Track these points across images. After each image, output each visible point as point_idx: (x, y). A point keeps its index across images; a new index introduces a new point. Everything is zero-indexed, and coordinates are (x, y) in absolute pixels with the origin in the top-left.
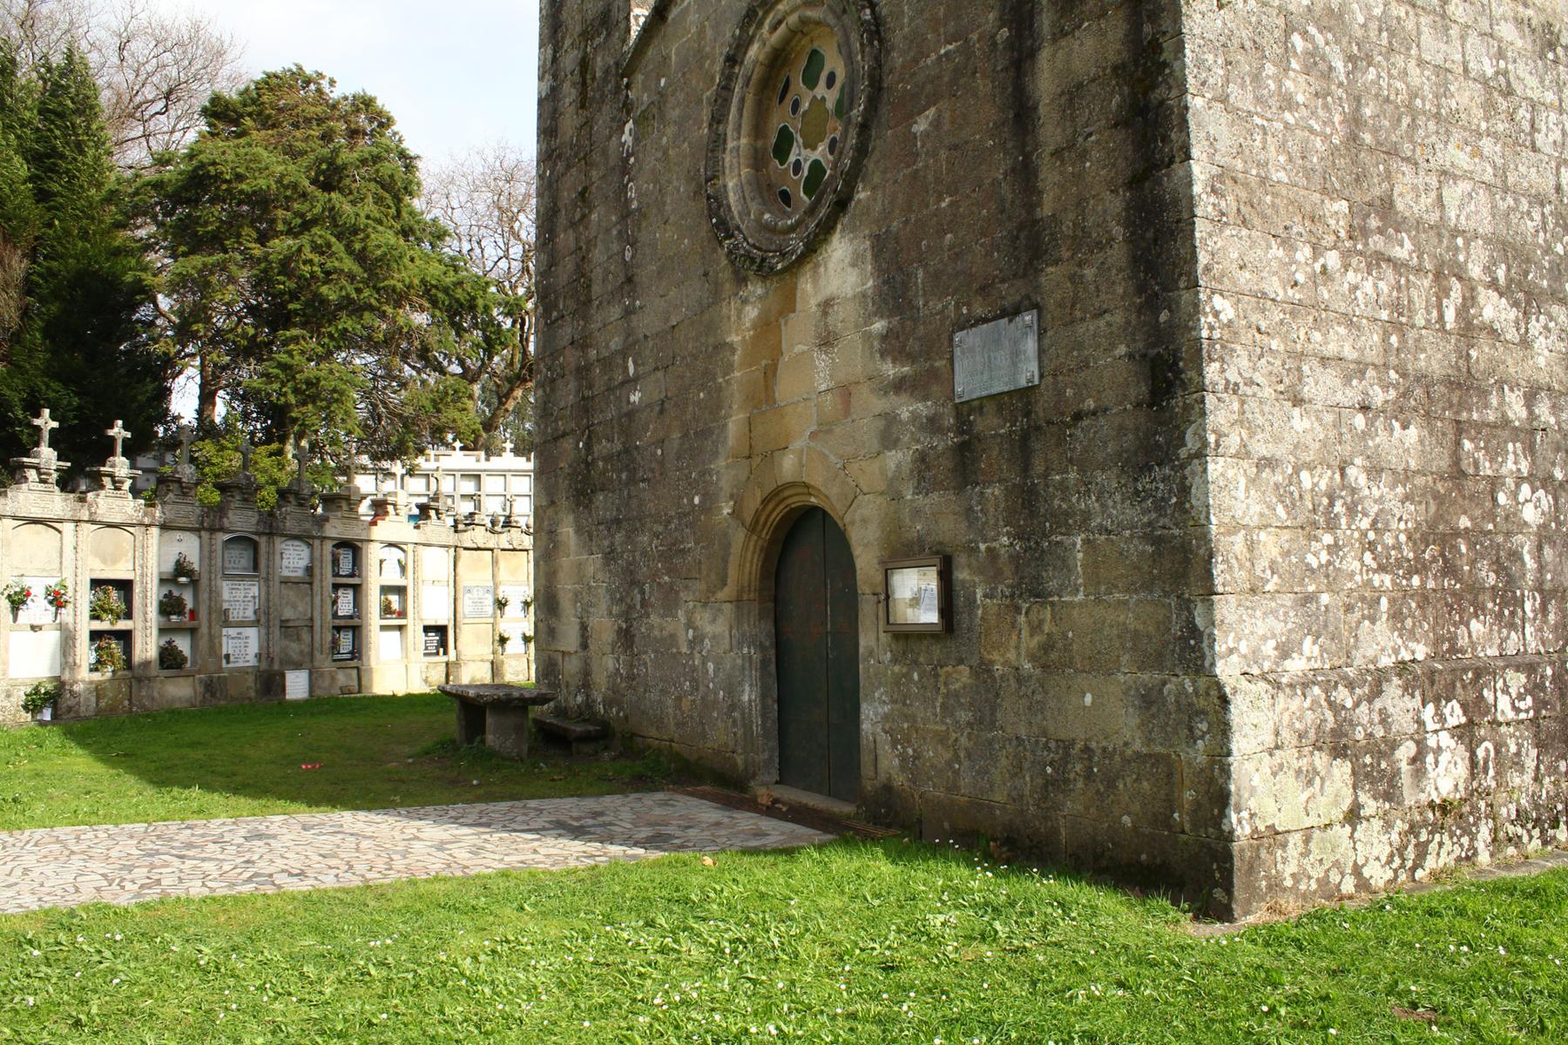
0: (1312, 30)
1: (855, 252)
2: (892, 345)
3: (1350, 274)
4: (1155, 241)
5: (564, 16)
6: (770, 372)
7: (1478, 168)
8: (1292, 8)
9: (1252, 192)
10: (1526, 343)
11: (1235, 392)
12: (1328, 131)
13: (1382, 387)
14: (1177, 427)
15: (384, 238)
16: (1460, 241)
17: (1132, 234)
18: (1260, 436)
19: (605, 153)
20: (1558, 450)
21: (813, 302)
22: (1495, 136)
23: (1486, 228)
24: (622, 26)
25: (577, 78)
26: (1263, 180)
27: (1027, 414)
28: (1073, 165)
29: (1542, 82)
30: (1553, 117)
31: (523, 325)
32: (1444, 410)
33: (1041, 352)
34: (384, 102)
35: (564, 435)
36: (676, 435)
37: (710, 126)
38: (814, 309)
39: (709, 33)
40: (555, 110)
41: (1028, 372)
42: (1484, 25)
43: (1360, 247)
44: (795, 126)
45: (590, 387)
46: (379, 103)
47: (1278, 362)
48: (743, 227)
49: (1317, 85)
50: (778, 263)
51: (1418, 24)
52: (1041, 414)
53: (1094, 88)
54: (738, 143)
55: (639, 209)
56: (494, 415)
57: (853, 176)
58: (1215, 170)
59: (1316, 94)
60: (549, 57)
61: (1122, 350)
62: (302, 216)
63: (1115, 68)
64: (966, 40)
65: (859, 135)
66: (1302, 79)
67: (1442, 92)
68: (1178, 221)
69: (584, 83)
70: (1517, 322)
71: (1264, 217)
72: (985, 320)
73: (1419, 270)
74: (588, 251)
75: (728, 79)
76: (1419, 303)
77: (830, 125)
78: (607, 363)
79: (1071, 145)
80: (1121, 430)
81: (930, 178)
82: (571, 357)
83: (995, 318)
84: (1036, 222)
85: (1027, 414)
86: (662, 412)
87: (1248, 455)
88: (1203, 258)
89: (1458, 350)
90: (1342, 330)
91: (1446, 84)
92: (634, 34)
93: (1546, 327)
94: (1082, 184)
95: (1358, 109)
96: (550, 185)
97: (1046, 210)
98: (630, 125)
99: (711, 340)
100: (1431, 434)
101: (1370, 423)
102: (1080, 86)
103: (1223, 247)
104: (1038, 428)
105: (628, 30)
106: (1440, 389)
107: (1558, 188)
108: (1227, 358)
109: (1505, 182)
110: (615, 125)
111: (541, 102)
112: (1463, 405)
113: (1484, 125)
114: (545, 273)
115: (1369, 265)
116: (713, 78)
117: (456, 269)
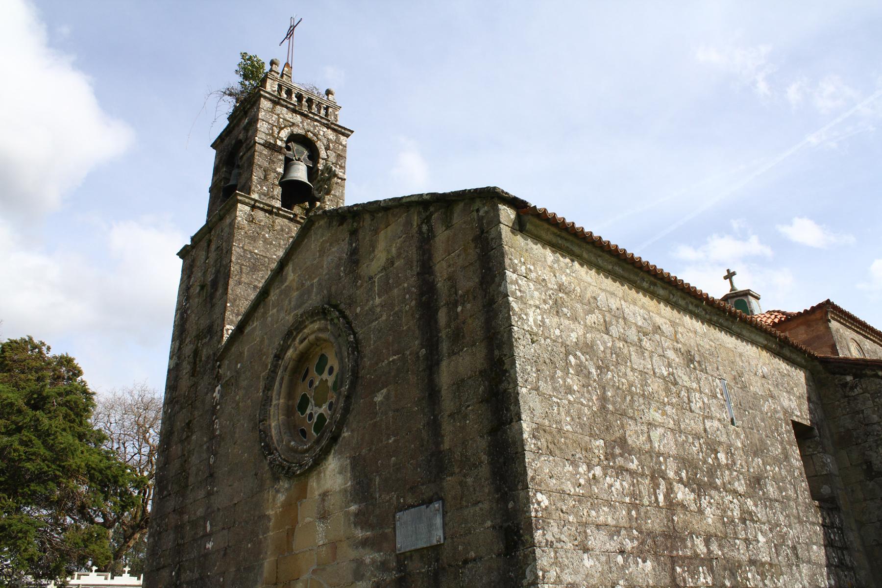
0: (579, 354)
1: (341, 466)
2: (361, 519)
3: (608, 478)
4: (505, 463)
5: (187, 326)
6: (291, 533)
7: (666, 421)
8: (568, 343)
9: (554, 437)
10: (701, 511)
11: (551, 547)
12: (591, 404)
13: (630, 540)
14: (521, 568)
15: (66, 439)
16: (661, 459)
17: (492, 459)
18: (567, 571)
19: (203, 402)
20: (725, 569)
21: (317, 493)
22: (672, 404)
23: (673, 452)
24: (219, 334)
25: (191, 360)
26: (560, 430)
27: (437, 560)
28: (460, 422)
29: (690, 378)
30: (697, 395)
31: (145, 494)
32: (664, 550)
33: (444, 525)
34: (79, 362)
35: (164, 567)
36: (233, 569)
37: (264, 391)
38: (317, 497)
39: (266, 342)
40: (177, 376)
41: (438, 535)
42: (660, 351)
43: (611, 464)
44: (311, 395)
45: (183, 538)
46: (75, 362)
47: (574, 529)
48: (279, 449)
49: (583, 381)
50: (298, 470)
51: (629, 351)
52: (445, 561)
53: (470, 382)
54: (279, 401)
55: (220, 435)
56: (120, 549)
57: (341, 424)
58: (534, 426)
59: (583, 386)
60: (177, 347)
61: (489, 523)
62: (16, 423)
63: (481, 372)
64: (403, 354)
65: (345, 401)
66: (575, 378)
67: (645, 384)
68: (517, 453)
69: (195, 363)
70: (695, 500)
71: (561, 449)
72: (413, 506)
73: (643, 475)
74: (189, 457)
75: (275, 367)
76: (645, 493)
77: (329, 395)
78: (194, 524)
79: (459, 412)
81: (383, 426)
82: (172, 519)
83: (419, 505)
84: (440, 452)
85: (437, 560)
86: (225, 555)
87: (561, 582)
88: (530, 473)
89: (667, 517)
90: (606, 509)
91: (646, 380)
92: (226, 337)
93: (709, 502)
94: (463, 433)
95: (604, 393)
96: (170, 418)
97: (446, 446)
98: (218, 388)
99: (257, 513)
100: (658, 565)
101: (626, 560)
102: (463, 380)
103: (540, 467)
104: (444, 569)
105: (222, 336)
106: (660, 539)
107: (705, 430)
108: (546, 527)
109: (680, 427)
110: (210, 387)
111: (169, 371)
112: (673, 548)
113: (666, 400)
114: (163, 466)
115: (617, 474)
116: (267, 365)
117: (108, 459)
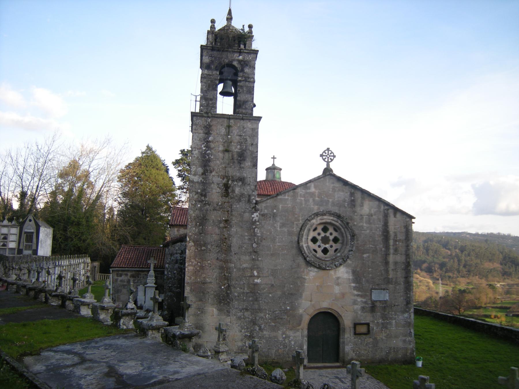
80: (401, 308)
